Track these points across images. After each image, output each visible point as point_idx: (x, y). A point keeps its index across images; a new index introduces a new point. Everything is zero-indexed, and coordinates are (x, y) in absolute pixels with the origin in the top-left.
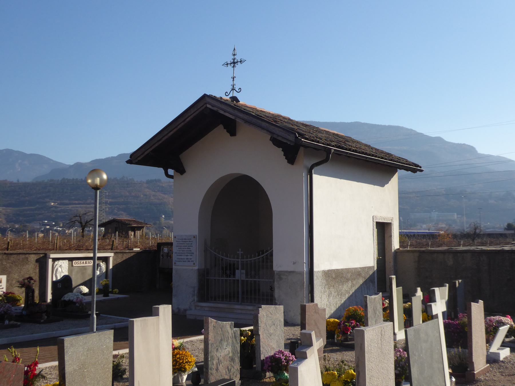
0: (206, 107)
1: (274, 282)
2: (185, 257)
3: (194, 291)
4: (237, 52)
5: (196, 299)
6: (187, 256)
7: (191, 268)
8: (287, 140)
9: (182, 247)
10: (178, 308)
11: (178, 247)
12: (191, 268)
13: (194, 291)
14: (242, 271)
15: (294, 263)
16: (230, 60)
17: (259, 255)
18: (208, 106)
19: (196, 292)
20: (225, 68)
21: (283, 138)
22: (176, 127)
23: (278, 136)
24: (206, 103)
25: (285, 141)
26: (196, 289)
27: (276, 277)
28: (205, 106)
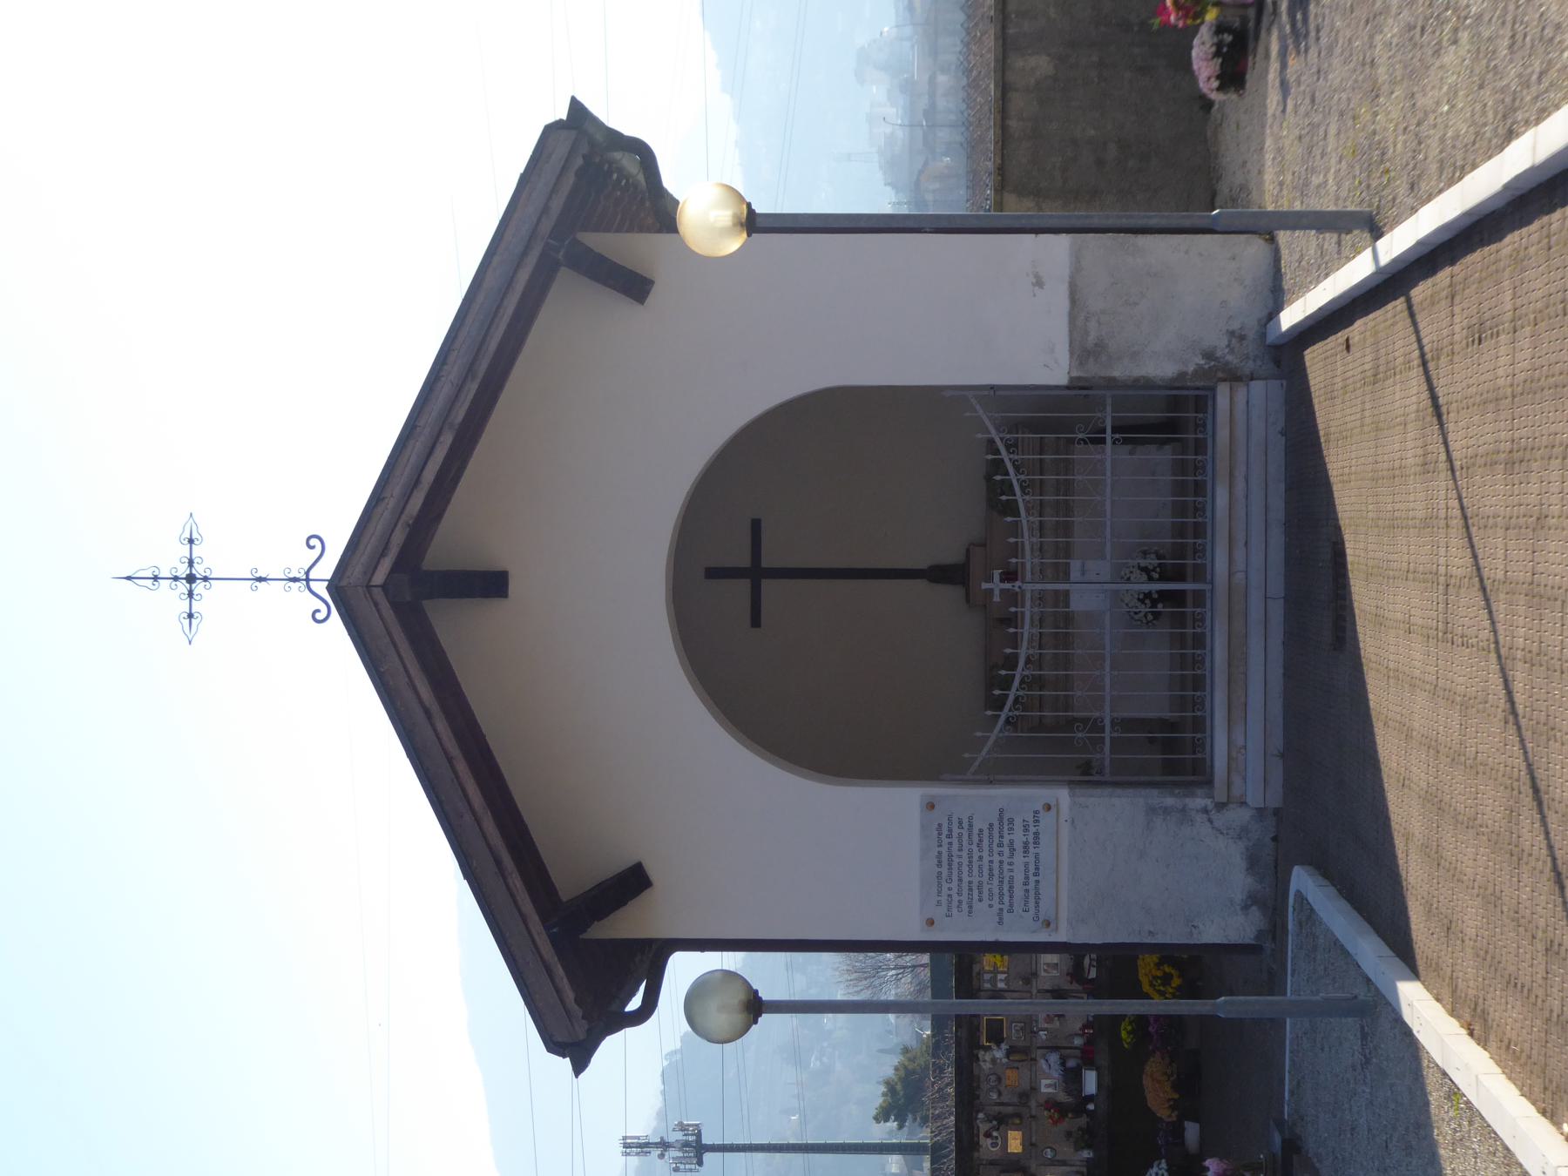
0: (384, 587)
1: (1111, 383)
2: (1019, 859)
3: (1166, 811)
4: (143, 567)
5: (1198, 801)
6: (1012, 850)
7: (1065, 830)
8: (564, 169)
9: (976, 880)
10: (1245, 908)
11: (977, 905)
12: (1065, 830)
13: (1166, 811)
14: (1075, 574)
15: (1039, 283)
16: (172, 597)
17: (1011, 508)
18: (379, 577)
19: (1169, 801)
20: (203, 627)
21: (554, 191)
22: (450, 760)
23: (545, 210)
24: (369, 587)
25: (570, 179)
26: (1156, 797)
27: (1093, 370)
28: (379, 595)
